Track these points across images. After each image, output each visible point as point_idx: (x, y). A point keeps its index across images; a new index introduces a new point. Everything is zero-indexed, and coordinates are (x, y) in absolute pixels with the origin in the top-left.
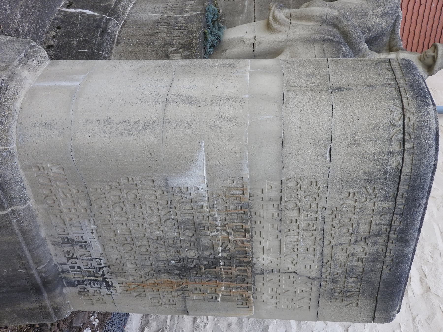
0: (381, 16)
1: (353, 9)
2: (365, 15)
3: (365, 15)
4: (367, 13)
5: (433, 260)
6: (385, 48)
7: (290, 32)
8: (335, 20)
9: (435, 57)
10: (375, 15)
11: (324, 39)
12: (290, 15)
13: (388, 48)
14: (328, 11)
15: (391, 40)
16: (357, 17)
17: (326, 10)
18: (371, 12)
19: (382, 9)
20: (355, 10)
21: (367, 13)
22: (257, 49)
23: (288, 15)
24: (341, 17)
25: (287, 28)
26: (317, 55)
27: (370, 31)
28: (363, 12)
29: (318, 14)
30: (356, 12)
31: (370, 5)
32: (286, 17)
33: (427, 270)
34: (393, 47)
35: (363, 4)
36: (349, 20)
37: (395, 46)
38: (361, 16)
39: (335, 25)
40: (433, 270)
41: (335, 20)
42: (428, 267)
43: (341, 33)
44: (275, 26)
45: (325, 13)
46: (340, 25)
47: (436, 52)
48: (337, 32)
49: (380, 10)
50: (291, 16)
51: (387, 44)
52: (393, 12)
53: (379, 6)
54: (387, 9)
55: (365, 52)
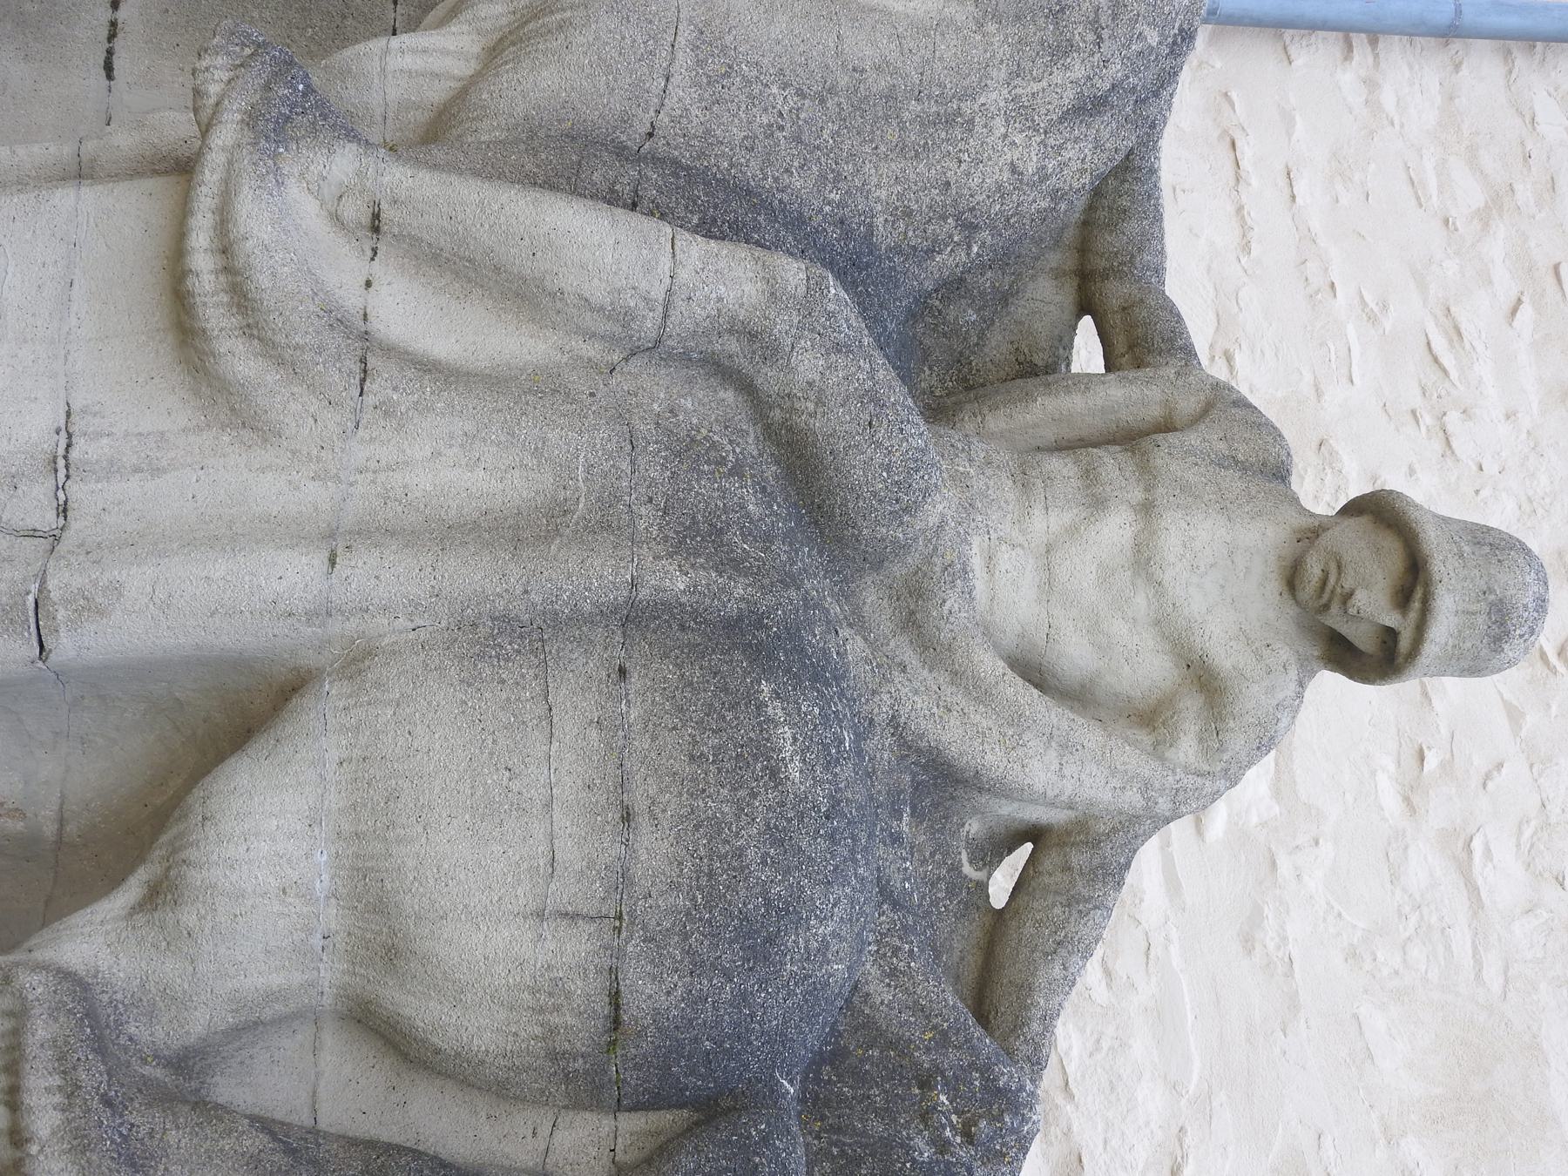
0: (1061, 120)
1: (871, 75)
2: (949, 121)
3: (949, 121)
4: (967, 108)
5: (1109, 986)
6: (1054, 259)
7: (360, 453)
8: (733, 345)
9: (1404, 644)
10: (1020, 112)
11: (632, 603)
12: (366, 219)
13: (1071, 263)
14: (684, 275)
15: (1102, 214)
16: (892, 134)
17: (665, 264)
18: (995, 97)
19: (1079, 72)
20: (883, 83)
21: (967, 108)
22: (65, 647)
23: (355, 211)
24: (783, 324)
25: (332, 420)
26: (568, 852)
27: (970, 228)
28: (941, 100)
29: (598, 292)
30: (890, 96)
31: (999, 40)
32: (336, 218)
33: (1075, 1052)
34: (1105, 276)
35: (942, 25)
36: (838, 348)
37: (1119, 274)
38: (924, 122)
39: (722, 371)
40: (1105, 1045)
41: (733, 345)
42: (1082, 1031)
43: (770, 432)
44: (240, 361)
45: (658, 293)
46: (769, 379)
47: (1416, 605)
48: (743, 421)
49: (1064, 83)
50: (376, 229)
51: (1070, 235)
52: (1150, 75)
53: (1061, 51)
54: (1116, 70)
55: (928, 559)
